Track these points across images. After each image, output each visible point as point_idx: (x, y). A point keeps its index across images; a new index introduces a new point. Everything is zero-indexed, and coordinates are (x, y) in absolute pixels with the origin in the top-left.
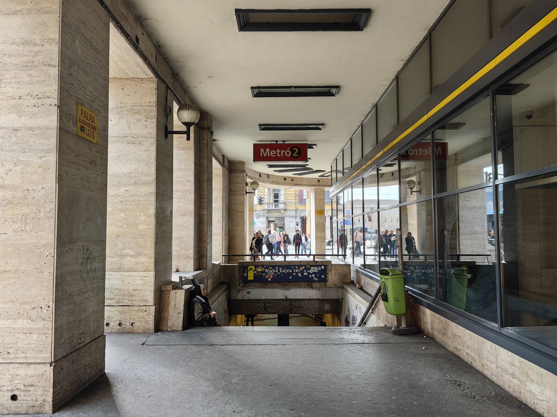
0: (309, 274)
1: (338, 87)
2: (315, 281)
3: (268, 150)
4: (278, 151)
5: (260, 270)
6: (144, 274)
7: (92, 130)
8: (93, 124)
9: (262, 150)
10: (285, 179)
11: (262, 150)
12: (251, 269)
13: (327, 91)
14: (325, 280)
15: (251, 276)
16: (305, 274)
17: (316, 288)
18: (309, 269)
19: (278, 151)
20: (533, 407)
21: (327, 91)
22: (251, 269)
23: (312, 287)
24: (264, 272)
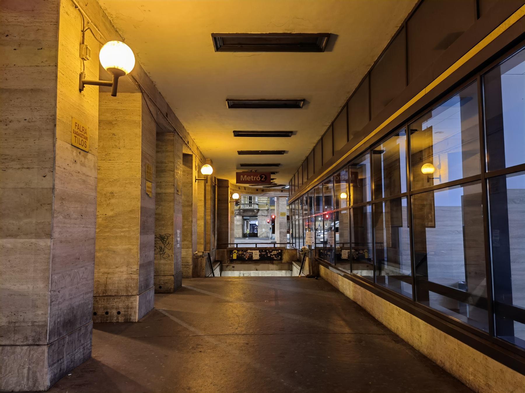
0: (271, 255)
1: (304, 100)
2: (275, 260)
3: (245, 176)
4: (252, 177)
5: (240, 253)
6: (187, 250)
7: (84, 140)
8: (85, 135)
9: (242, 176)
10: (257, 190)
11: (242, 176)
12: (235, 252)
13: (293, 104)
14: (281, 259)
15: (235, 256)
16: (269, 255)
17: (276, 264)
18: (271, 252)
19: (252, 177)
20: (457, 375)
21: (293, 104)
22: (235, 252)
23: (273, 264)
24: (243, 254)
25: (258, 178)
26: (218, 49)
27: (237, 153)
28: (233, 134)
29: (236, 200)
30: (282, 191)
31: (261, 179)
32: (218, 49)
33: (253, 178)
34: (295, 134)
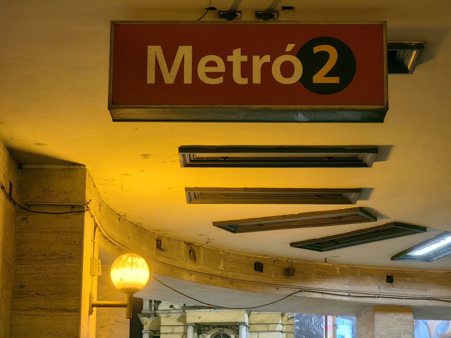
3: (185, 52)
4: (237, 57)
9: (155, 52)
11: (155, 52)
19: (237, 57)
25: (287, 69)
26: (190, 201)
27: (183, 196)
28: (177, 157)
29: (130, 291)
30: (390, 279)
31: (309, 72)
32: (190, 201)
33: (247, 70)
34: (384, 158)
